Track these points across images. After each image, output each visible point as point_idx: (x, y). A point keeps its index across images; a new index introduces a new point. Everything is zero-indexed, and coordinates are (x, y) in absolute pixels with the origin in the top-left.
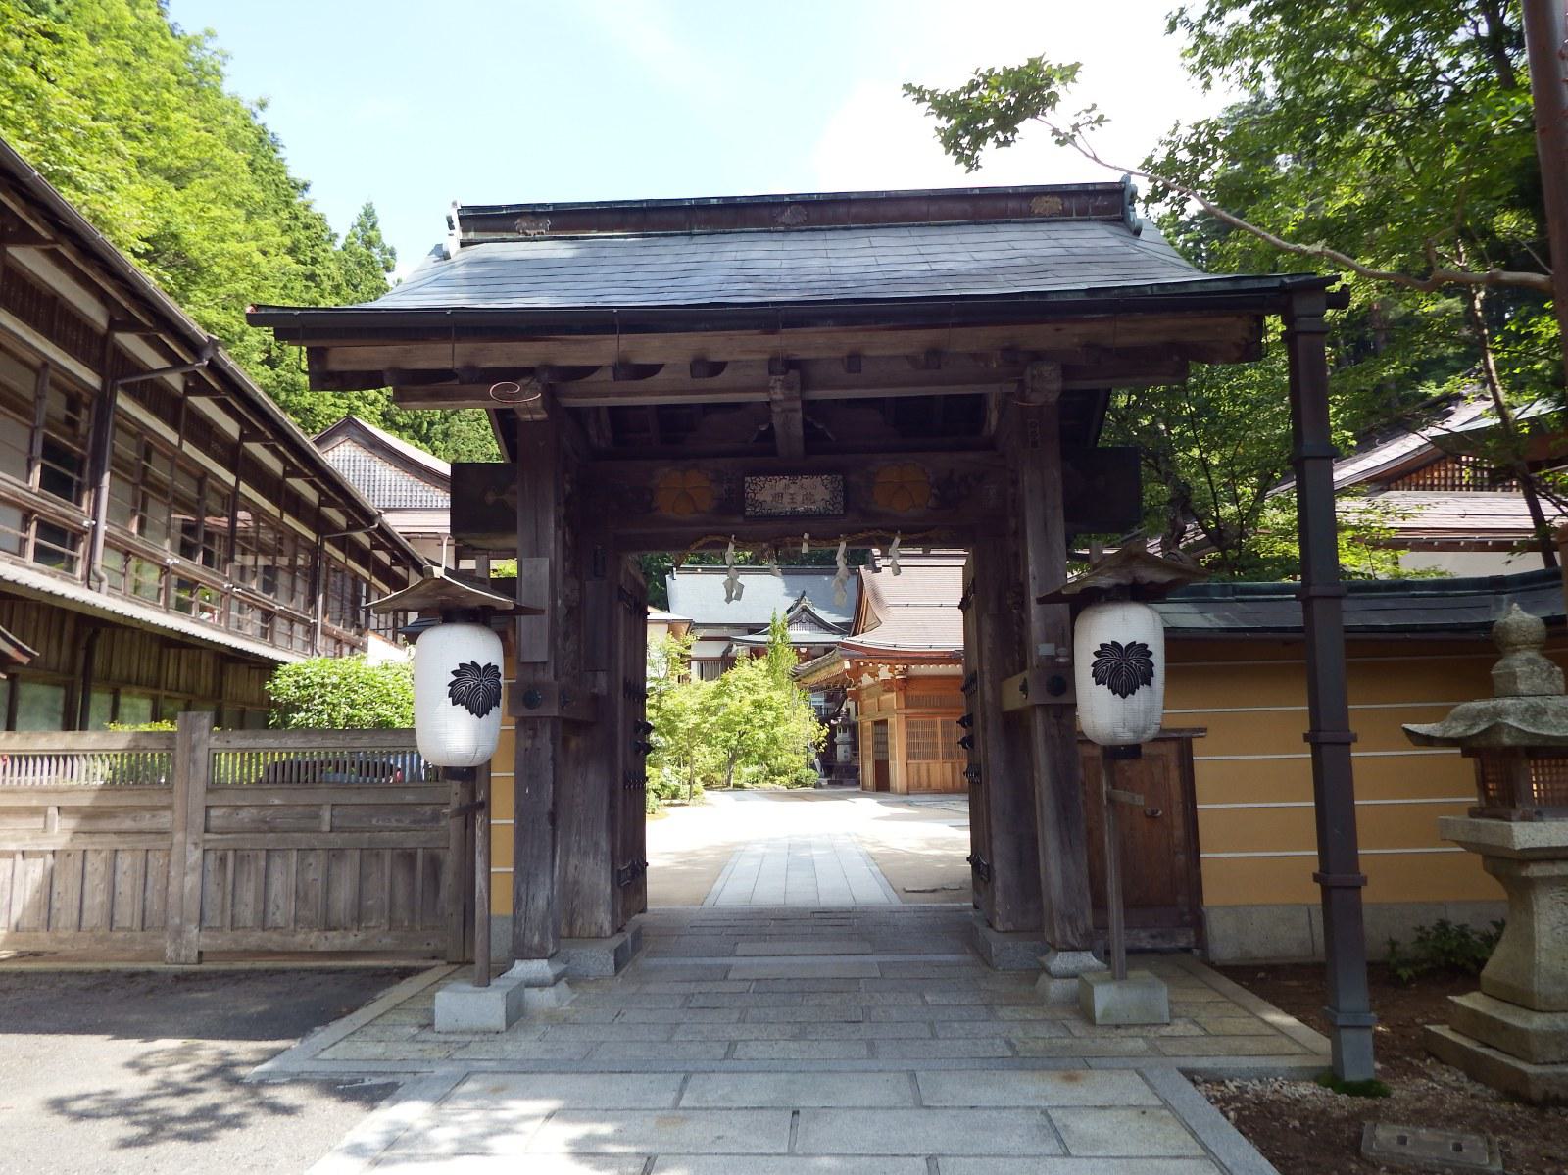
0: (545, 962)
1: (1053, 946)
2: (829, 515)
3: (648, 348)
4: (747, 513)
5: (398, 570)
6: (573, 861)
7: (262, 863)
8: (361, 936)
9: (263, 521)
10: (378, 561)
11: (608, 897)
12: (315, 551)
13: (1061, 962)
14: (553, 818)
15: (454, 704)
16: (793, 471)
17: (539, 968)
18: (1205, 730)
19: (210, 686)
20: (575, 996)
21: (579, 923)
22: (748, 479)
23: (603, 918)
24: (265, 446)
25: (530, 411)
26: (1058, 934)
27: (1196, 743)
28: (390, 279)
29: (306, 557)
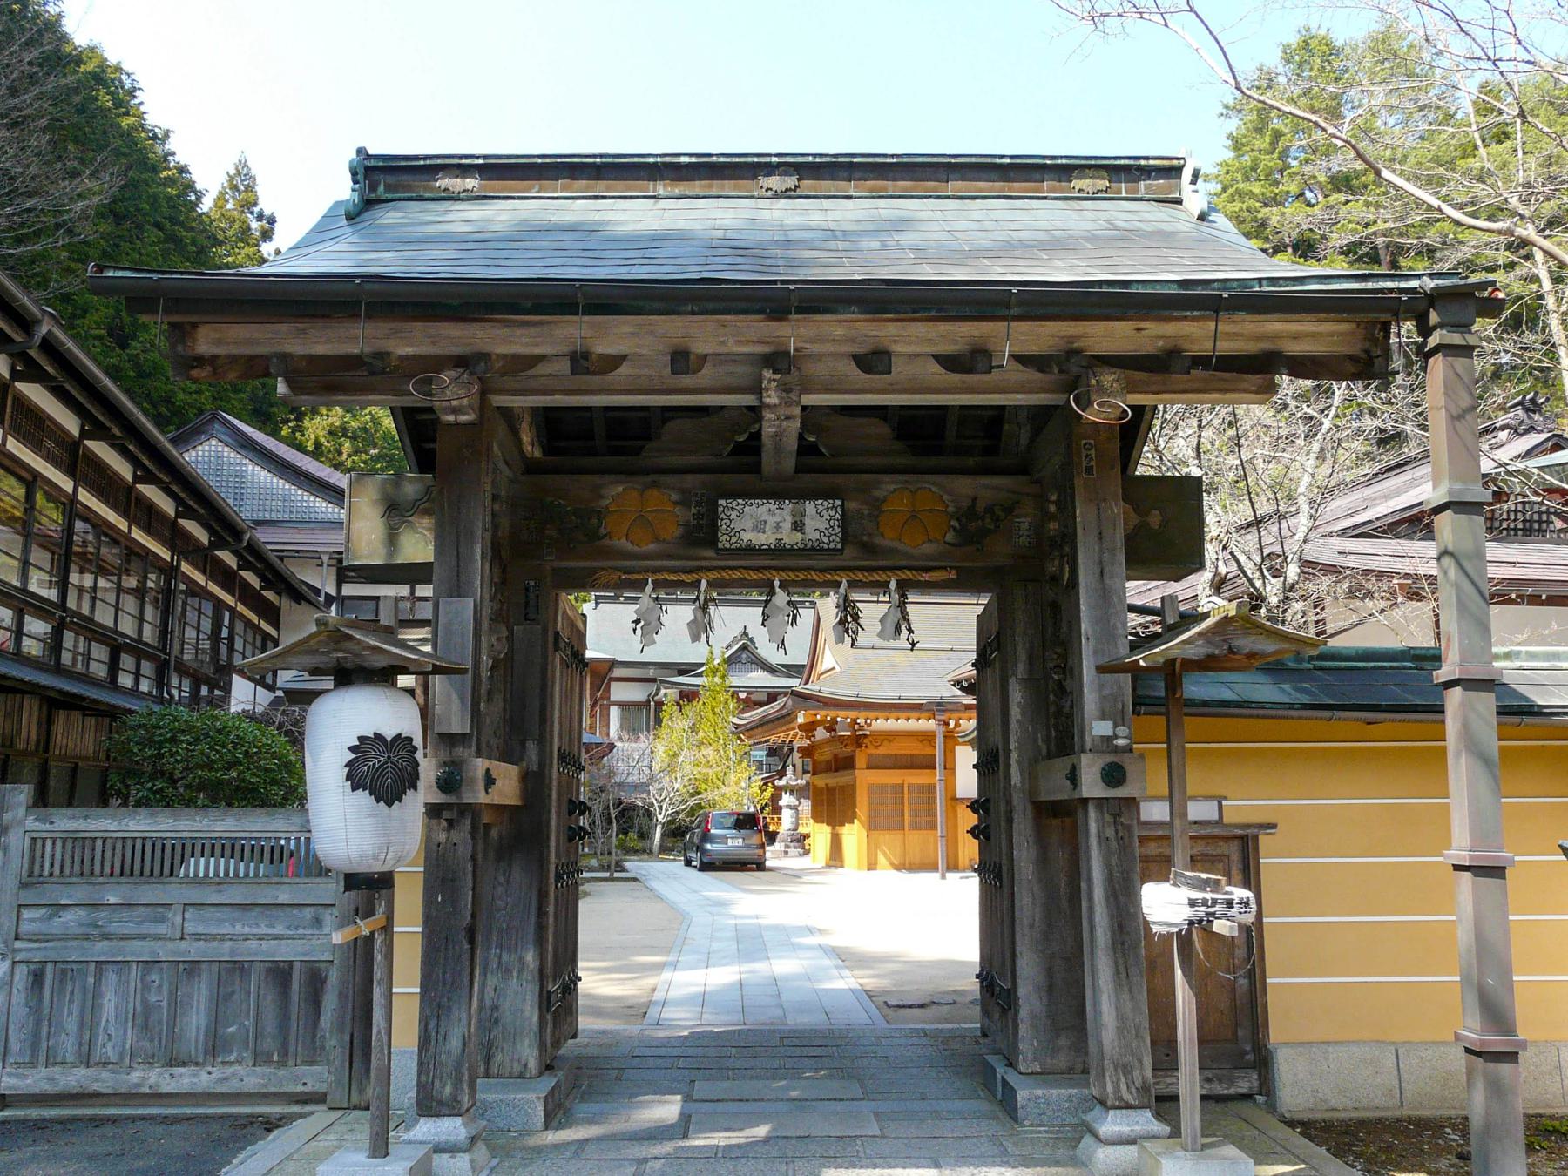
0: (458, 1121)
1: (1103, 1103)
2: (822, 549)
3: (615, 336)
4: (720, 545)
5: (269, 595)
6: (492, 981)
7: (91, 980)
8: (217, 1073)
9: (106, 535)
10: (245, 585)
11: (535, 1028)
12: (170, 572)
13: (1113, 1124)
14: (471, 933)
15: (353, 790)
16: (776, 492)
17: (451, 1128)
18: (1274, 826)
19: (33, 736)
20: (496, 1161)
21: (498, 1058)
22: (722, 502)
23: (529, 1054)
24: (112, 446)
25: (455, 411)
26: (1110, 1089)
27: (1264, 841)
28: (267, 249)
29: (159, 578)
